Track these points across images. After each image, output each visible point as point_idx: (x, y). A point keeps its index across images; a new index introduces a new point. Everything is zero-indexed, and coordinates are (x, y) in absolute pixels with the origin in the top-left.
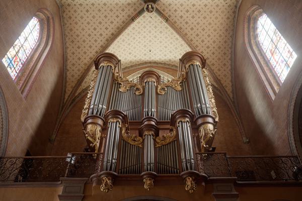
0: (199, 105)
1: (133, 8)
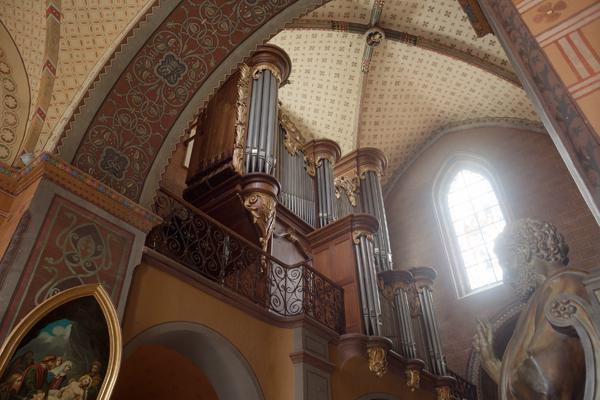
1: (348, 10)
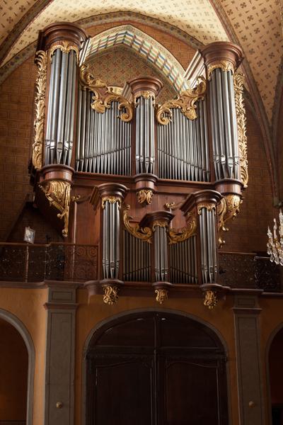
0: (223, 159)
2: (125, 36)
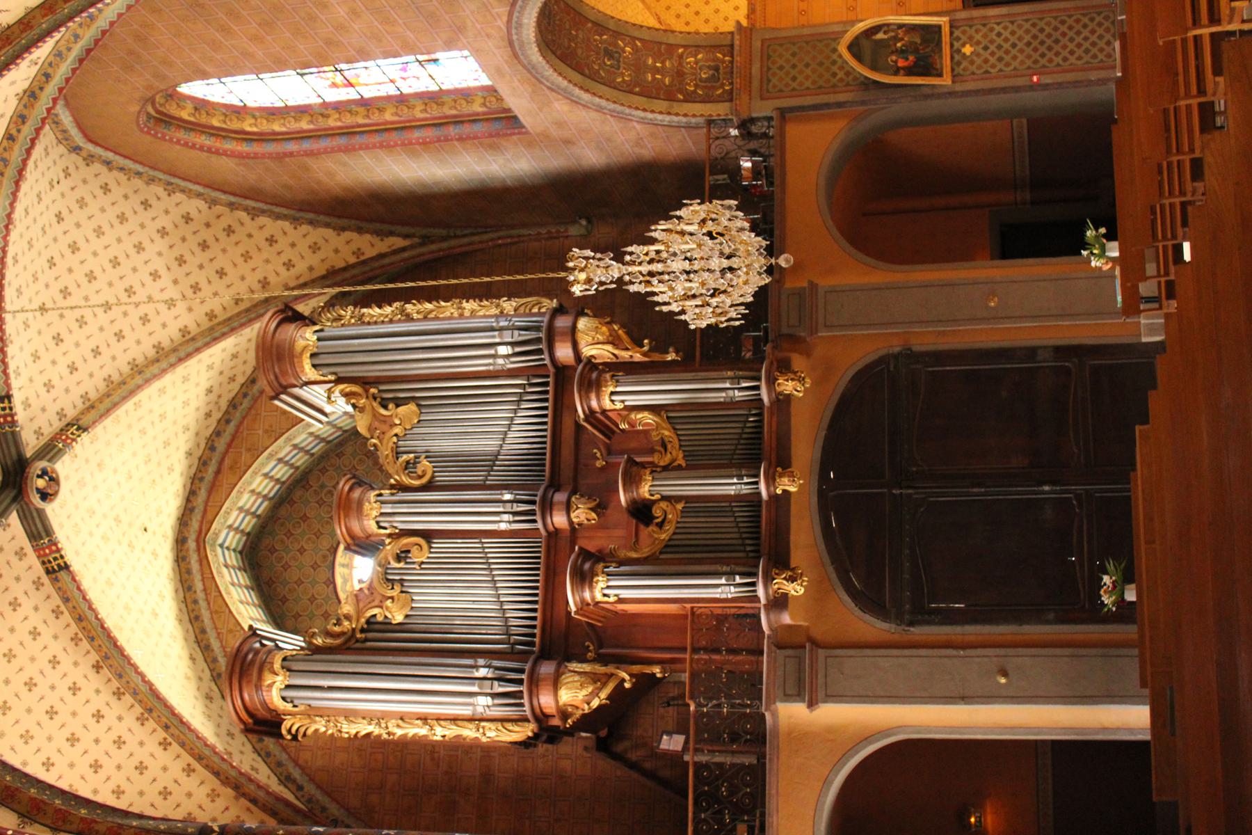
2: (228, 548)
